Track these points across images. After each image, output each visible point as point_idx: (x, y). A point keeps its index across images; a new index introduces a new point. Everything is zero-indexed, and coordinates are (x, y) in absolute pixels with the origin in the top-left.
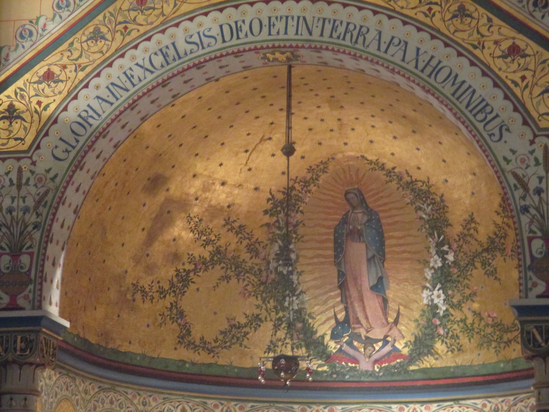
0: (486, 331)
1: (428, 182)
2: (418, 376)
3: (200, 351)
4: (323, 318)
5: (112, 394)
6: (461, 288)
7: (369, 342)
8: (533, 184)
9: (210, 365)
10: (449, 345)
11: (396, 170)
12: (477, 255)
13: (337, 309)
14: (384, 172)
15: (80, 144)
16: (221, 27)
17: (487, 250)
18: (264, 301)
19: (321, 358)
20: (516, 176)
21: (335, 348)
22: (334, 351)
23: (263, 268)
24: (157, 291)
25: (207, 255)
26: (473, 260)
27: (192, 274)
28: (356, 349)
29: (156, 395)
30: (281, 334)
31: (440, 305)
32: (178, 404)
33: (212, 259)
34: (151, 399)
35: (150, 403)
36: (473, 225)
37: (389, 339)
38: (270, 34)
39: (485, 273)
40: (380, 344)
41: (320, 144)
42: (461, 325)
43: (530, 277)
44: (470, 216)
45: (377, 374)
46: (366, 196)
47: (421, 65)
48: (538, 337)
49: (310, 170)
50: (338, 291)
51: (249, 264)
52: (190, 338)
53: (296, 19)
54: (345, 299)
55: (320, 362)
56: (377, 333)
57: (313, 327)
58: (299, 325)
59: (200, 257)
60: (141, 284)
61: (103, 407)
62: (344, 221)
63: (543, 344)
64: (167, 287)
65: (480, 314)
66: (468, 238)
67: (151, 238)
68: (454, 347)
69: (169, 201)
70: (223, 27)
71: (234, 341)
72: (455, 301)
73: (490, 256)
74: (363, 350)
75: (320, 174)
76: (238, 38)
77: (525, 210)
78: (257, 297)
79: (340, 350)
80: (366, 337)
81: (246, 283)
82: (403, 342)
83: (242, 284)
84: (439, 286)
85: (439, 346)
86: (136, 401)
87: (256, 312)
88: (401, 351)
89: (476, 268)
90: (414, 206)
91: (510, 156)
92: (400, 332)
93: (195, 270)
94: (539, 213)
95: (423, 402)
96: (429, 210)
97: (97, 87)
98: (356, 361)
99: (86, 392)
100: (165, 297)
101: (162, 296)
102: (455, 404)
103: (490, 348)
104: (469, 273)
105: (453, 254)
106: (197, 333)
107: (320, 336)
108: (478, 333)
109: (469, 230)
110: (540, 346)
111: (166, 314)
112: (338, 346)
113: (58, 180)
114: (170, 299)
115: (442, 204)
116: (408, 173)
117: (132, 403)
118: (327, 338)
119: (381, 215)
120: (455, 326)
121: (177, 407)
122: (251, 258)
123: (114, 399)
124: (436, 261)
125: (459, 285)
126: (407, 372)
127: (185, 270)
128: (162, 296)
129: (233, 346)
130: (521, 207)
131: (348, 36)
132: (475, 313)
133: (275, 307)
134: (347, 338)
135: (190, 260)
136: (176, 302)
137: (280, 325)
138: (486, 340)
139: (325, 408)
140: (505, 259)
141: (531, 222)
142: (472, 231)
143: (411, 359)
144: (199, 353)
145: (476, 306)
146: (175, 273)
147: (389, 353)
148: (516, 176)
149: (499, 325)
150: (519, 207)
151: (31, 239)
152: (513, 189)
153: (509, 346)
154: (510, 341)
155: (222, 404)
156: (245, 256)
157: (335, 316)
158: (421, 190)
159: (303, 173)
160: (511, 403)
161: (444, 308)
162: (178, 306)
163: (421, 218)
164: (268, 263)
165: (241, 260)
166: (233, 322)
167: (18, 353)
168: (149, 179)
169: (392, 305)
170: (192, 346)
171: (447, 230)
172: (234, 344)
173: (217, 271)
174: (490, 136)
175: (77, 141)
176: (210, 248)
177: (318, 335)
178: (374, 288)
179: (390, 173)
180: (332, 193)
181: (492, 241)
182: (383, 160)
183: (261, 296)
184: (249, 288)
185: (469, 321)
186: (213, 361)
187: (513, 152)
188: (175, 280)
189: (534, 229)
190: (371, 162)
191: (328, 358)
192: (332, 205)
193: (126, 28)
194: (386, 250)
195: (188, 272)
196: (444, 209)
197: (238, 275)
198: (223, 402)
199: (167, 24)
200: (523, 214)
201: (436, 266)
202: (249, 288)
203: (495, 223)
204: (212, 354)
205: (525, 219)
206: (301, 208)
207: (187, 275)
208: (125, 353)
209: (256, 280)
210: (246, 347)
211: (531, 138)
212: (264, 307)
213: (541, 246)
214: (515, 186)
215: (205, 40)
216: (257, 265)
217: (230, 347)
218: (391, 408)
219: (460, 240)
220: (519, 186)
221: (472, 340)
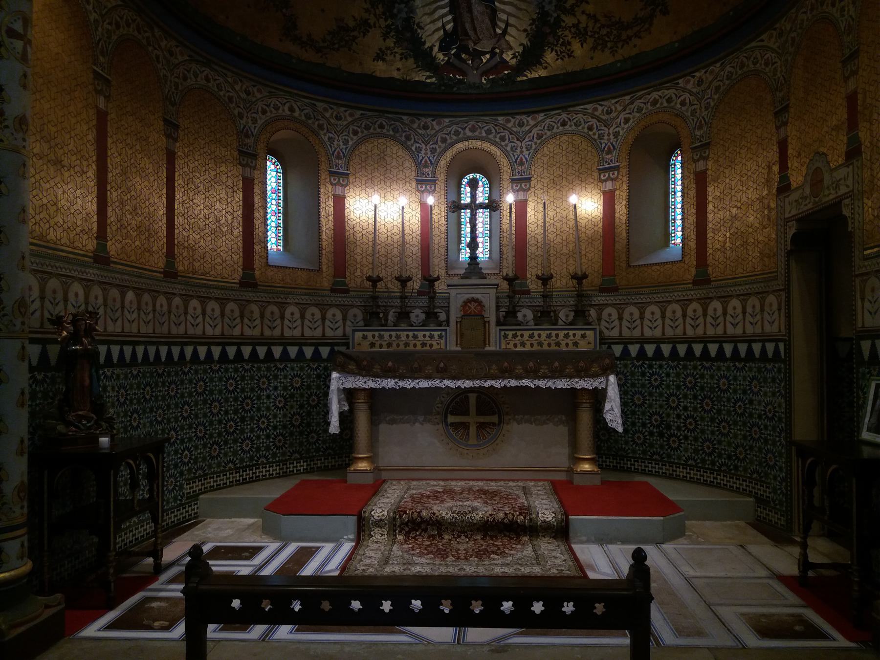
4: (432, 27)
10: (559, 53)
13: (446, 19)
21: (443, 60)
22: (442, 63)
28: (464, 61)
30: (390, 43)
35: (254, 93)
40: (488, 56)
42: (573, 30)
45: (484, 86)
55: (428, 73)
57: (421, 38)
58: (408, 35)
68: (564, 54)
79: (448, 62)
82: (510, 53)
85: (549, 57)
86: (237, 87)
88: (508, 62)
92: (507, 42)
95: (528, 114)
98: (463, 73)
102: (563, 111)
107: (428, 47)
108: (591, 36)
112: (446, 59)
118: (436, 49)
120: (567, 32)
121: (285, 104)
132: (589, 16)
134: (455, 50)
137: (389, 33)
143: (519, 70)
154: (630, 38)
155: (332, 108)
157: (443, 26)
177: (426, 46)
185: (582, 25)
198: (332, 106)
199: (316, 542)
210: (354, 52)
218: (497, 120)
221: (584, 45)
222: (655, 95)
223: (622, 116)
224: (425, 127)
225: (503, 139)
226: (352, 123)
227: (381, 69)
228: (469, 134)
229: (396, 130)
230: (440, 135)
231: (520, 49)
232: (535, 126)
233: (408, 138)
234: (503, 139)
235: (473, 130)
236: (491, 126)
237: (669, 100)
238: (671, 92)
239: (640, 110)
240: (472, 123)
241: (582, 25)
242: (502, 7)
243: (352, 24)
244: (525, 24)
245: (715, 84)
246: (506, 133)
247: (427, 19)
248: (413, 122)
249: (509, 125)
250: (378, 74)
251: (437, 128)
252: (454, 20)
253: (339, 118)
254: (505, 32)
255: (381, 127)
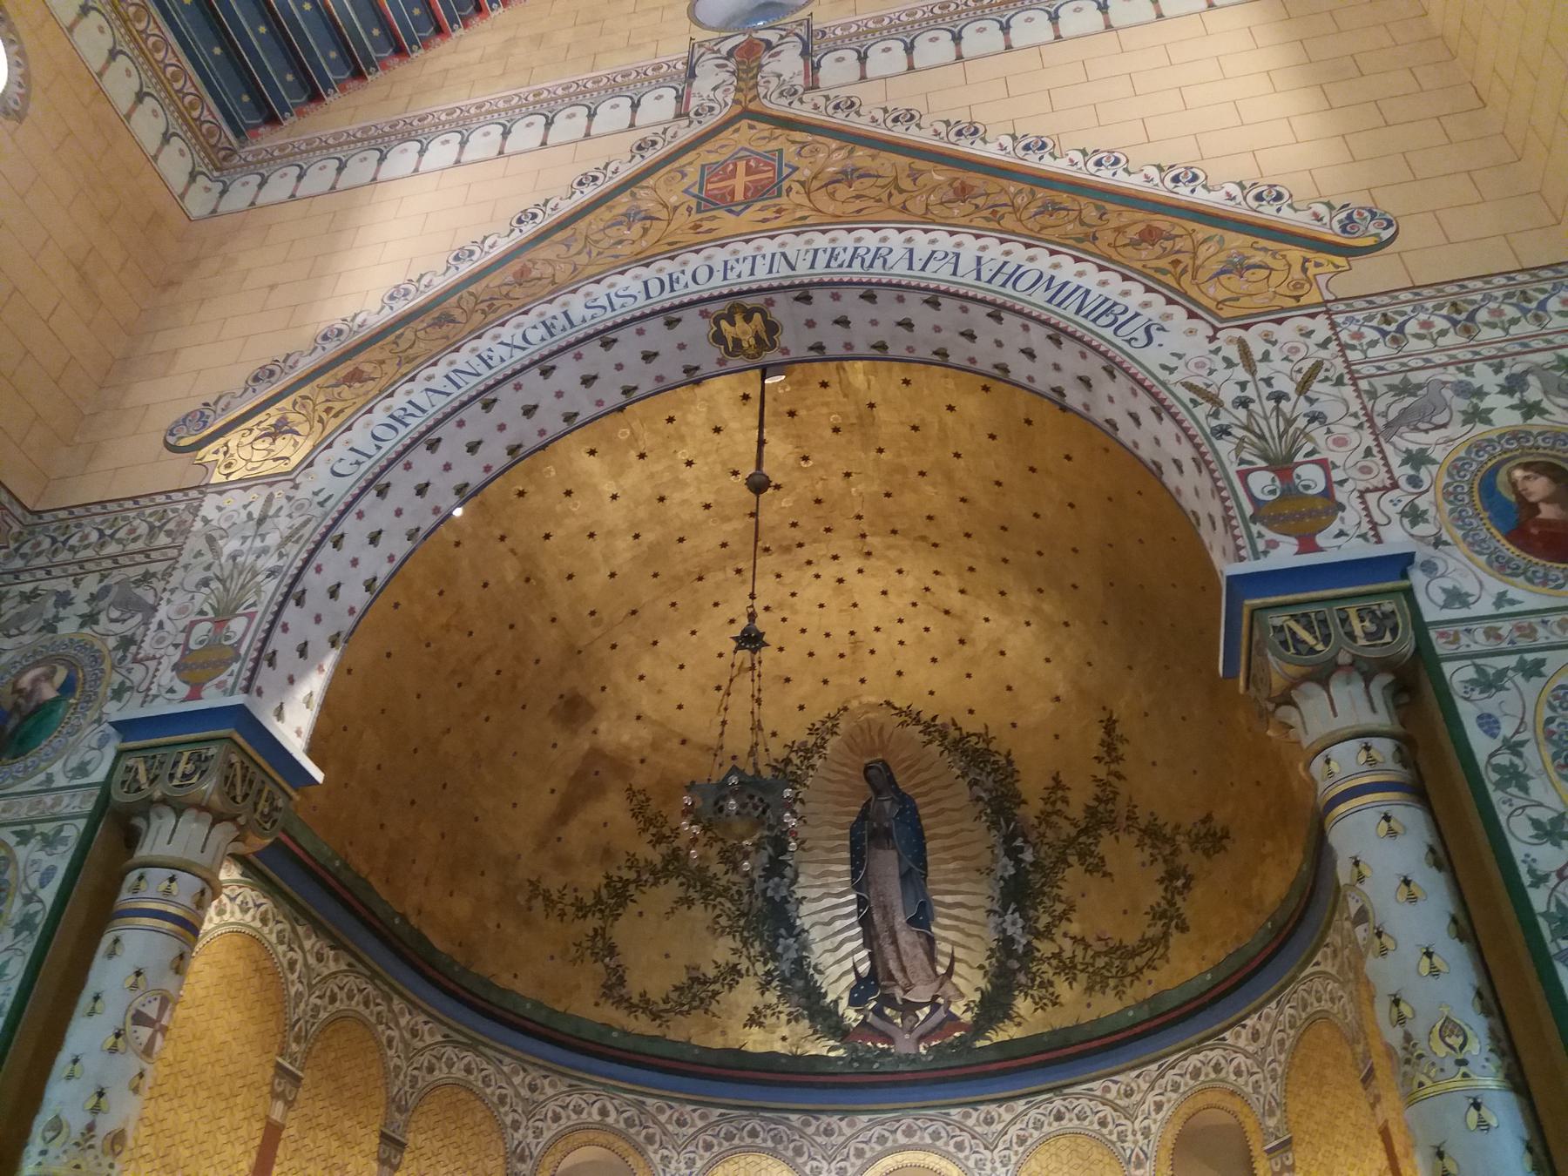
0: (1097, 965)
1: (987, 733)
2: (992, 1055)
3: (639, 1013)
4: (835, 971)
5: (470, 1057)
6: (1049, 903)
7: (909, 1008)
8: (1229, 394)
9: (653, 1039)
11: (938, 722)
12: (1071, 842)
14: (921, 728)
15: (383, 451)
16: (646, 283)
17: (1084, 831)
18: (745, 942)
19: (834, 1037)
20: (1190, 387)
21: (856, 1020)
22: (855, 1025)
23: (744, 890)
24: (572, 905)
25: (657, 860)
26: (1064, 853)
27: (632, 887)
28: (889, 1020)
29: (555, 1078)
30: (771, 997)
31: (1017, 937)
32: (595, 1098)
33: (665, 868)
34: (546, 1082)
35: (543, 1088)
36: (1060, 793)
37: (941, 1001)
38: (725, 278)
39: (1086, 871)
40: (927, 1010)
41: (825, 682)
42: (1054, 962)
43: (1259, 533)
44: (1054, 779)
46: (895, 771)
47: (986, 275)
48: (1304, 634)
49: (812, 730)
50: (859, 929)
51: (723, 882)
52: (624, 991)
53: (768, 258)
54: (870, 939)
55: (832, 1043)
56: (921, 993)
57: (820, 987)
58: (800, 983)
59: (646, 861)
60: (543, 886)
61: (449, 1072)
62: (864, 815)
63: (1320, 647)
64: (589, 901)
65: (1083, 939)
66: (1054, 818)
67: (565, 813)
69: (596, 754)
70: (649, 283)
71: (696, 1004)
72: (1041, 925)
73: (1091, 840)
74: (899, 1021)
75: (827, 737)
76: (672, 290)
77: (1223, 431)
78: (734, 937)
79: (864, 1023)
80: (903, 1000)
81: (718, 912)
82: (961, 1003)
83: (711, 914)
84: (1013, 906)
85: (1023, 1005)
86: (516, 1080)
87: (734, 959)
88: (959, 1019)
89: (1070, 866)
90: (967, 780)
91: (1172, 362)
93: (637, 882)
94: (1253, 432)
95: (1000, 1101)
96: (989, 783)
97: (429, 378)
98: (889, 1039)
99: (414, 1033)
100: (585, 916)
101: (580, 914)
103: (1107, 990)
104: (1060, 876)
105: (1031, 850)
106: (634, 988)
108: (1082, 971)
109: (1054, 803)
110: (1312, 651)
111: (585, 945)
112: (861, 1017)
113: (329, 504)
114: (593, 922)
115: (1010, 769)
116: (954, 724)
117: (511, 1083)
118: (844, 1003)
119: (918, 801)
120: (1045, 967)
122: (726, 873)
123: (474, 1066)
124: (1005, 867)
125: (1045, 900)
126: (971, 1050)
127: (621, 878)
128: (580, 914)
129: (693, 1012)
130: (1212, 429)
131: (857, 262)
132: (1074, 939)
133: (762, 954)
134: (874, 1003)
135: (629, 864)
136: (604, 929)
138: (1098, 979)
139: (841, 1120)
140: (1117, 838)
141: (1239, 449)
142: (1059, 805)
144: (636, 1017)
145: (1075, 928)
146: (605, 881)
147: (940, 1025)
148: (1190, 387)
149: (1118, 949)
150: (1208, 431)
151: (258, 592)
152: (1191, 406)
153: (1138, 978)
154: (1140, 970)
155: (671, 1107)
156: (717, 868)
158: (977, 750)
159: (802, 736)
160: (1155, 1075)
161: (1024, 941)
162: (607, 936)
163: (979, 799)
164: (753, 882)
165: (710, 874)
166: (694, 974)
167: (176, 782)
168: (562, 696)
169: (943, 947)
170: (624, 1002)
171: (1020, 811)
172: (695, 1008)
173: (672, 889)
174: (1129, 341)
175: (379, 448)
176: (663, 848)
177: (828, 1000)
178: (911, 922)
179: (929, 727)
180: (846, 769)
181: (1091, 811)
182: (916, 707)
183: (741, 934)
184: (723, 921)
185: (1067, 954)
186: (657, 1032)
187: (1180, 356)
188: (604, 892)
189: (1246, 456)
190: (900, 712)
191: (838, 1030)
192: (846, 789)
193: (490, 306)
194: (929, 858)
195: (627, 883)
196: (1012, 776)
197: (705, 898)
198: (673, 1104)
200: (1220, 438)
201: (1006, 875)
202: (723, 921)
203: (1095, 779)
204: (658, 1022)
205: (1225, 447)
206: (800, 796)
207: (624, 887)
208: (503, 990)
209: (733, 908)
211: (1211, 333)
212: (745, 952)
213: (1269, 482)
214: (1192, 401)
215: (617, 302)
216: (734, 884)
217: (688, 1012)
219: (1040, 824)
220: (1200, 400)
221: (1074, 984)
222: (1194, 1060)
223: (1151, 1099)
224: (828, 1132)
225: (960, 1147)
226: (703, 1130)
227: (756, 1041)
228: (902, 1140)
229: (777, 1139)
230: (853, 1145)
231: (977, 997)
232: (1013, 1122)
233: (798, 1152)
234: (960, 1147)
235: (909, 1132)
236: (938, 1125)
237: (1217, 1068)
238: (1216, 1055)
239: (1176, 1087)
240: (907, 1121)
241: (1067, 954)
242: (943, 933)
243: (711, 973)
244: (981, 958)
245: (1277, 1036)
246: (966, 1137)
247: (828, 959)
248: (807, 1124)
249: (970, 1122)
250: (750, 1048)
251: (848, 1132)
252: (871, 956)
253: (681, 1123)
254: (950, 971)
255: (753, 1134)
